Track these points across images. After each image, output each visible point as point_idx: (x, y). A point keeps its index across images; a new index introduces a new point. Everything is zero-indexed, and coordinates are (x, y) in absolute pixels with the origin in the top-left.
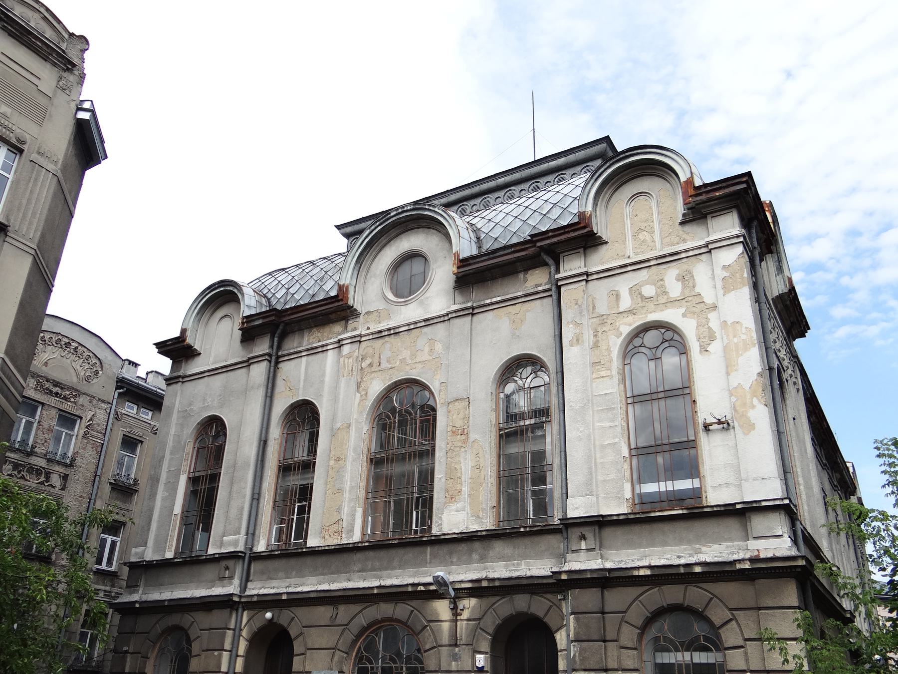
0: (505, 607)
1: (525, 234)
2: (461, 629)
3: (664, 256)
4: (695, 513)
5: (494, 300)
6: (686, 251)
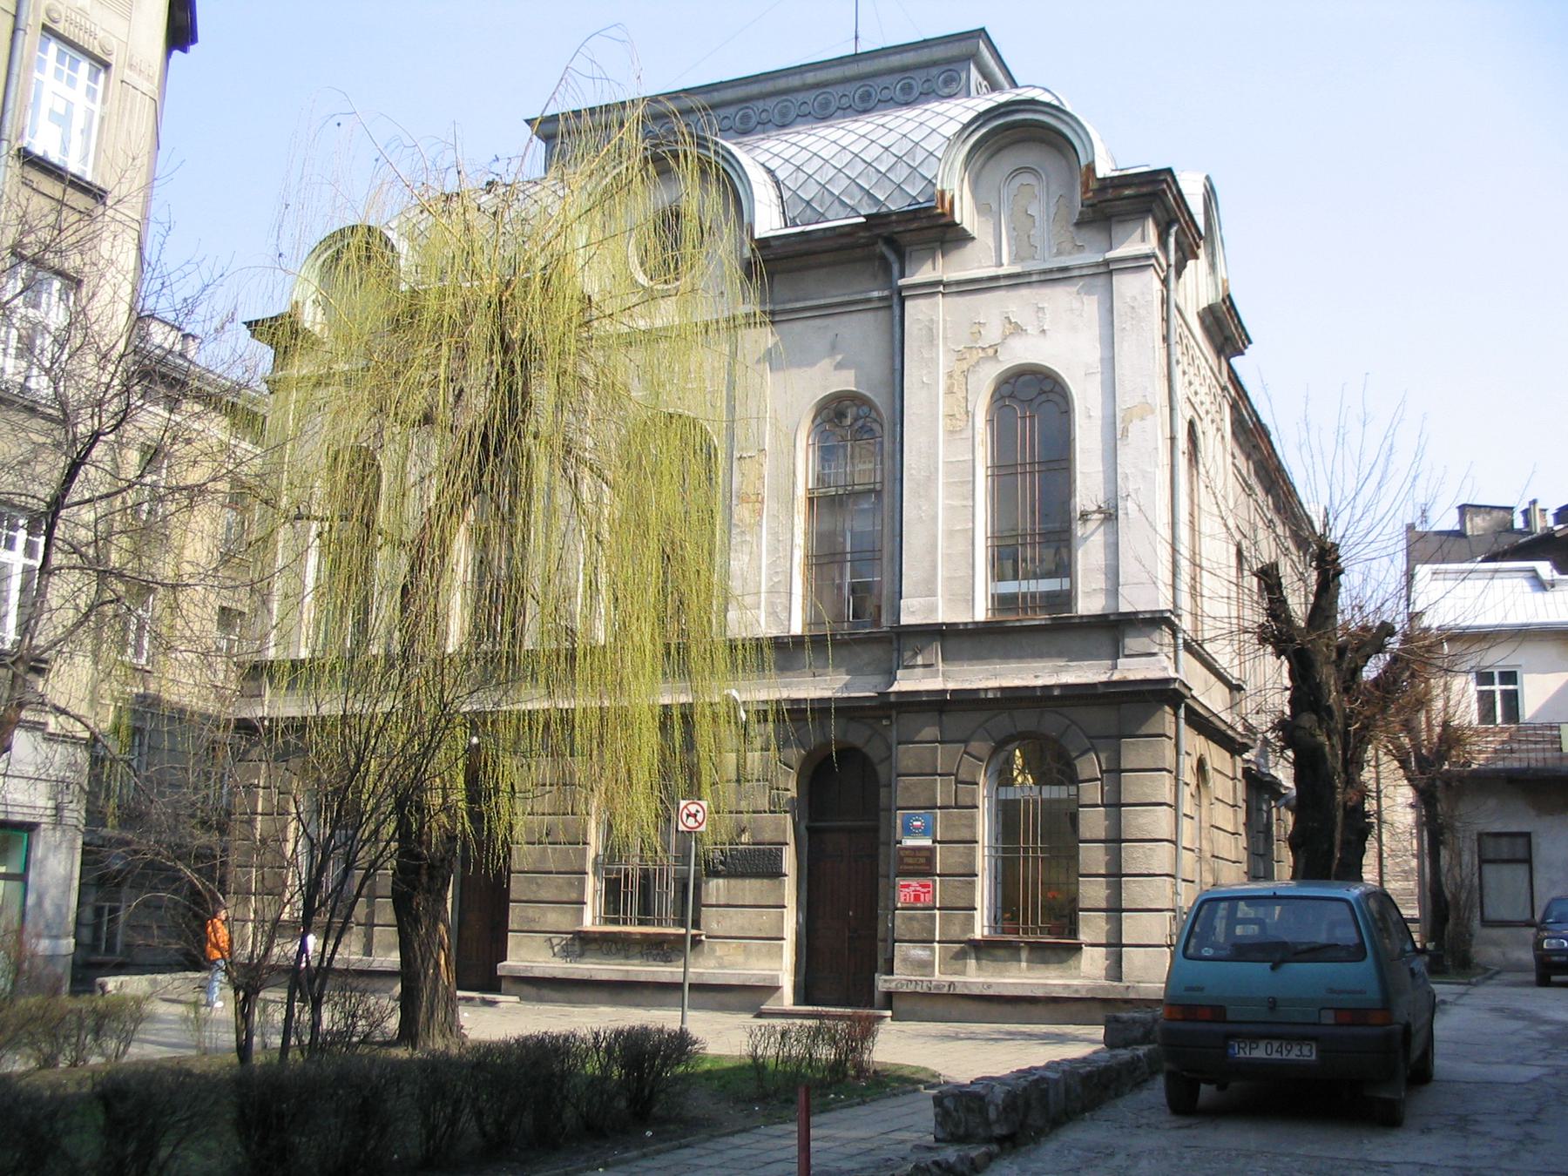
3: (1051, 271)
4: (1062, 628)
5: (809, 303)
6: (1081, 267)
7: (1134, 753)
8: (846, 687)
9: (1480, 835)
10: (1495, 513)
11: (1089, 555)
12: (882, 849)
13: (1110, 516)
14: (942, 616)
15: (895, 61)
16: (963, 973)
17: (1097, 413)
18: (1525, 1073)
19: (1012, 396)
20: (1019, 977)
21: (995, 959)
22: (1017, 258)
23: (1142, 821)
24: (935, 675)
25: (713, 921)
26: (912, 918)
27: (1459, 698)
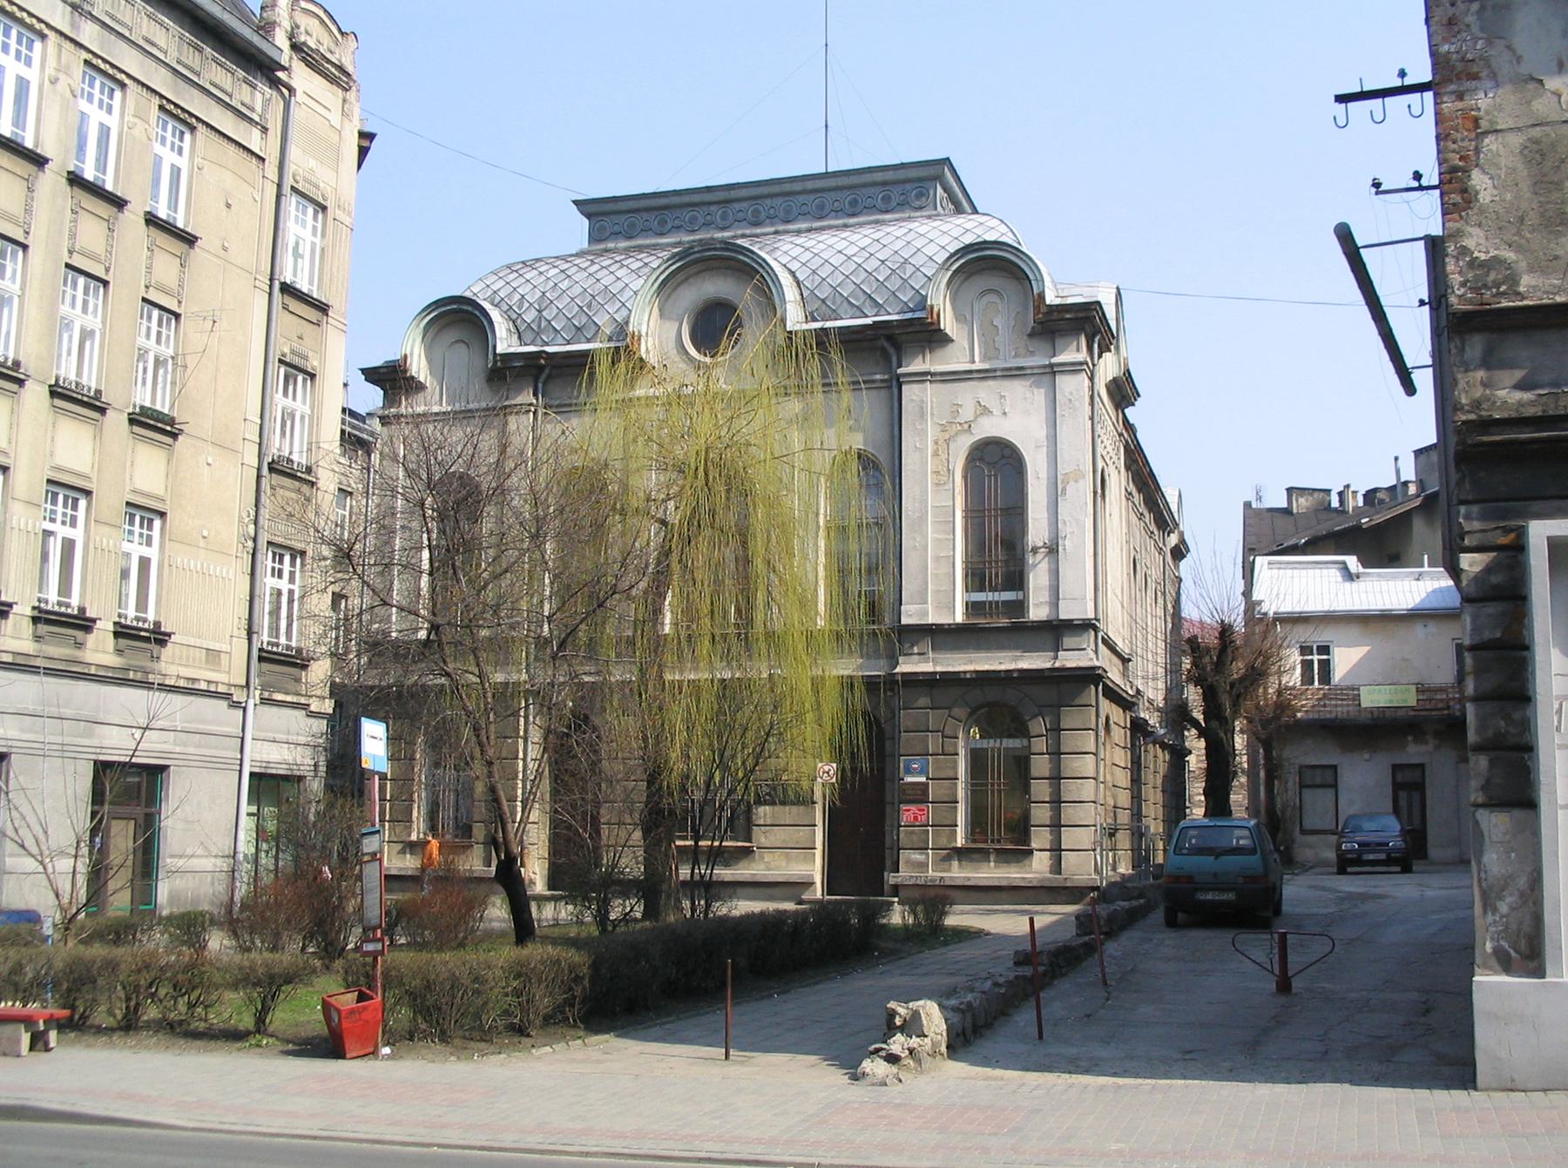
3: (1010, 369)
7: (1069, 718)
8: (860, 667)
9: (1301, 767)
10: (1316, 495)
11: (1038, 577)
12: (888, 784)
13: (1053, 550)
14: (931, 619)
15: (878, 177)
16: (949, 870)
17: (1043, 475)
18: (1325, 911)
19: (981, 459)
20: (990, 873)
21: (972, 860)
22: (984, 358)
23: (1072, 765)
24: (927, 661)
25: (760, 837)
26: (912, 832)
27: (1290, 671)
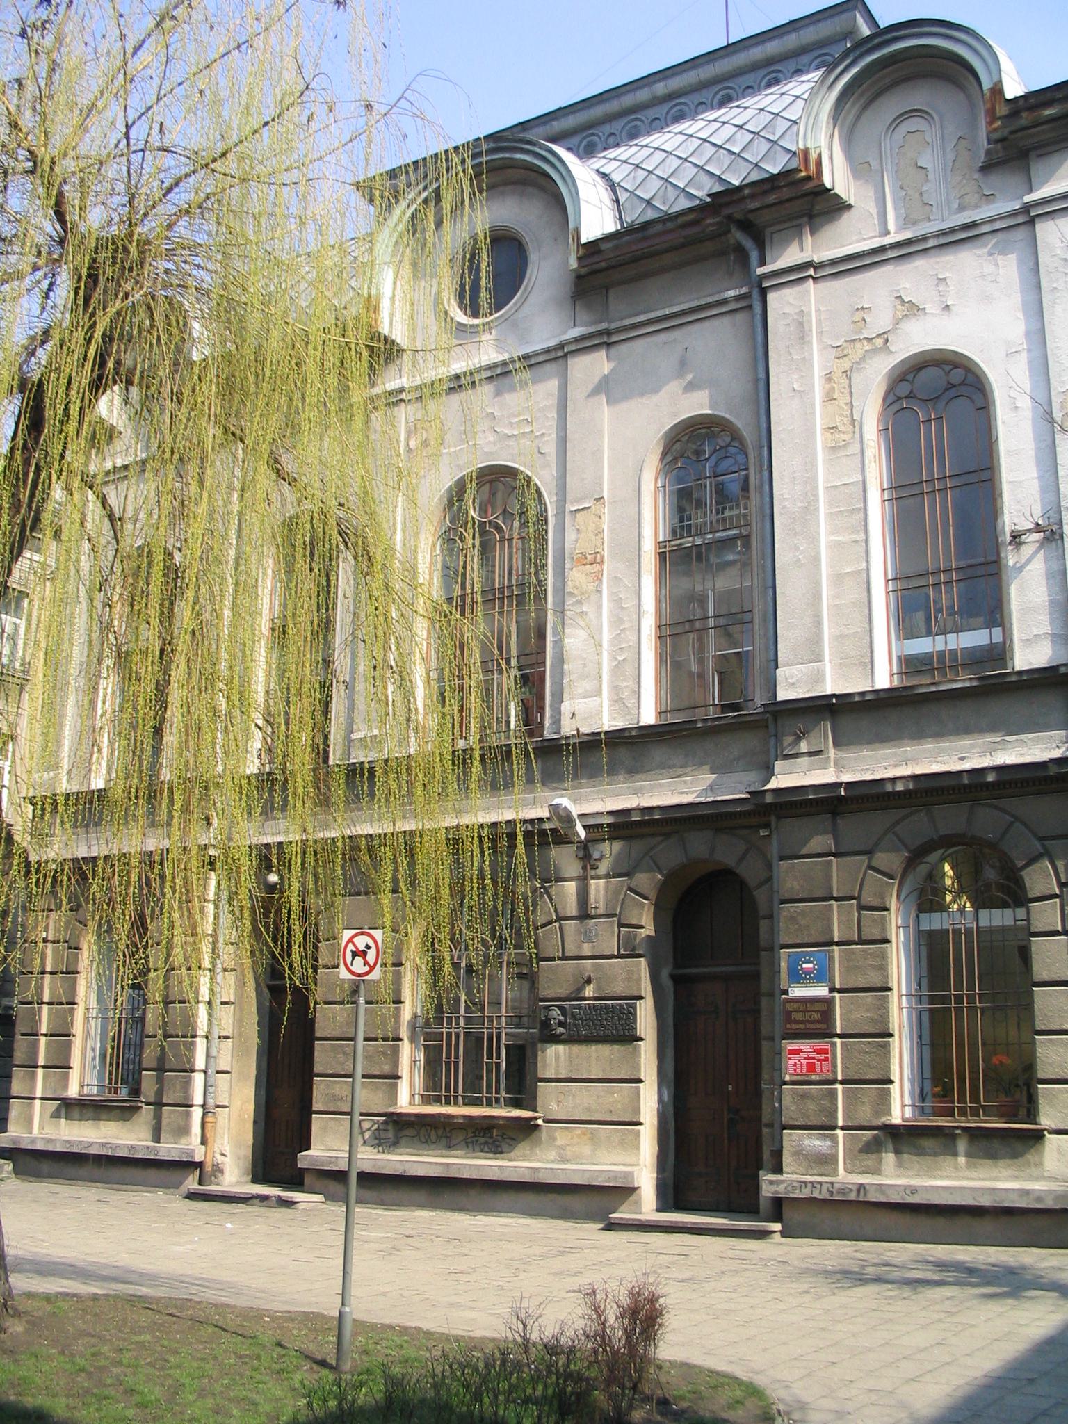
0: (672, 854)
1: (703, 190)
2: (597, 891)
3: (952, 231)
6: (991, 221)
12: (764, 1002)
14: (830, 687)
16: (877, 1171)
21: (921, 1153)
24: (825, 767)
25: (552, 1101)
26: (805, 1096)
